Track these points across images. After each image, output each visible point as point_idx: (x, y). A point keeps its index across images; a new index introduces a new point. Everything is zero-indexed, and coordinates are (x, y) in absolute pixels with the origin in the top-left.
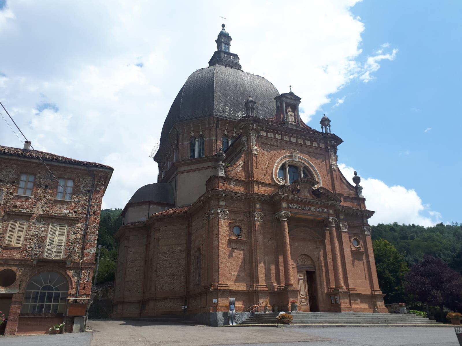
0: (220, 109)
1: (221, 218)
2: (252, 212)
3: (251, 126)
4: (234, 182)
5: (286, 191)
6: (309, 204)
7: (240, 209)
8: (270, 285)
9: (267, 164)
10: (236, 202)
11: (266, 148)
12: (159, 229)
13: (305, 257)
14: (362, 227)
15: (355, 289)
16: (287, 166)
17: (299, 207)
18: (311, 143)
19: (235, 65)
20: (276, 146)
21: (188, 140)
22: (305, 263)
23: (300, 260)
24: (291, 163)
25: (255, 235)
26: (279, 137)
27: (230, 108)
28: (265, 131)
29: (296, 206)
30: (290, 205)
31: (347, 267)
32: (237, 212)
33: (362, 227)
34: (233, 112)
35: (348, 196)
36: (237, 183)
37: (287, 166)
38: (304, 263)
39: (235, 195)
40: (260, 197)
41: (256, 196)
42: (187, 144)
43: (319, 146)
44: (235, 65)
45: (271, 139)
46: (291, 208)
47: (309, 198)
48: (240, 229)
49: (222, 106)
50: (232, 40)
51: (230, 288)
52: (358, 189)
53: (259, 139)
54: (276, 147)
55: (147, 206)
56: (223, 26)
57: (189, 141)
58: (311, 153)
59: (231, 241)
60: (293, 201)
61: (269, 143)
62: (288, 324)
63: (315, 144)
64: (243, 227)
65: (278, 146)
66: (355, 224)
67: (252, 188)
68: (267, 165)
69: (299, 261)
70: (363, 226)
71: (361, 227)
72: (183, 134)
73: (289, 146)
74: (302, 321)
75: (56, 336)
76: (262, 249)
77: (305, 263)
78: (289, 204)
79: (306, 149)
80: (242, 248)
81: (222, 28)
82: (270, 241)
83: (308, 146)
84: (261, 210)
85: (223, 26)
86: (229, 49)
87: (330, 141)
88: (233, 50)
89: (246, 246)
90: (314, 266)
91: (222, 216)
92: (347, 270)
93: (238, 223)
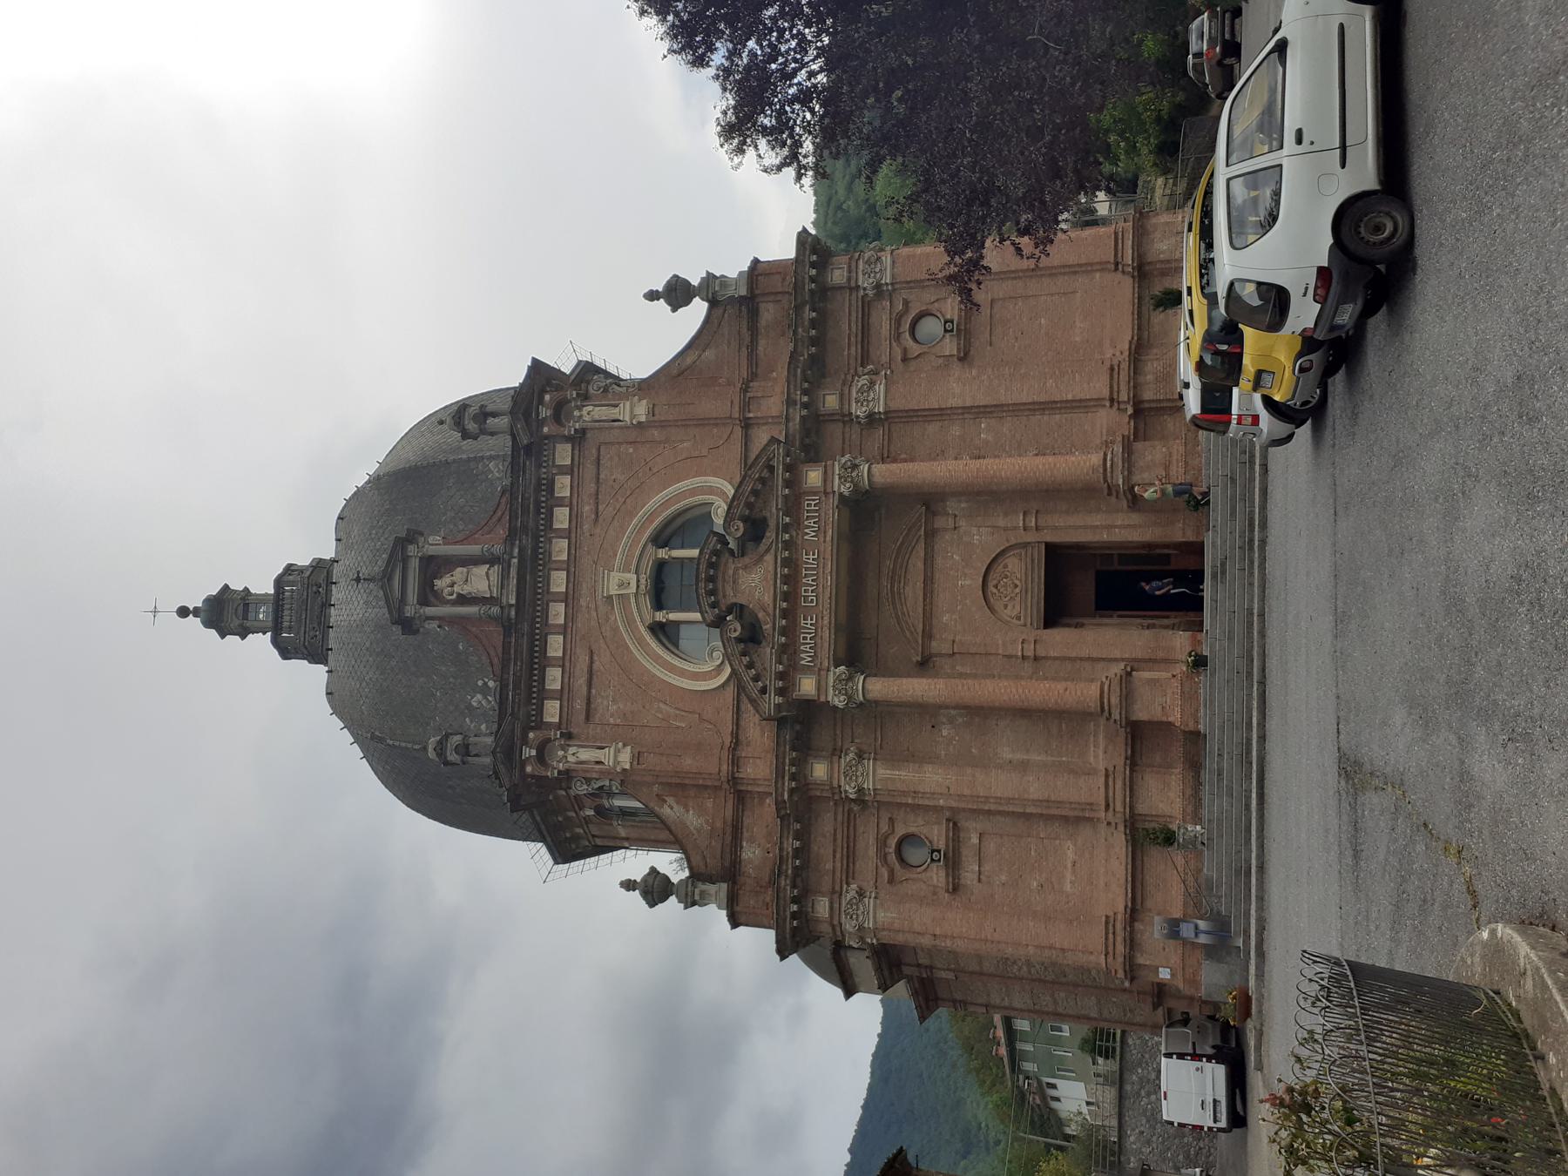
0: (483, 727)
1: (875, 922)
2: (843, 796)
3: (533, 769)
4: (741, 847)
5: (756, 679)
6: (792, 564)
7: (839, 836)
8: (1105, 752)
9: (662, 705)
10: (816, 848)
11: (605, 703)
12: (926, 967)
13: (995, 582)
14: (862, 292)
15: (1112, 369)
16: (660, 616)
17: (809, 622)
18: (560, 502)
19: (315, 588)
20: (592, 662)
21: (612, 825)
22: (1016, 586)
23: (1006, 607)
24: (647, 603)
25: (928, 796)
26: (555, 645)
27: (476, 690)
28: (545, 671)
29: (809, 636)
30: (805, 660)
31: (1025, 397)
32: (848, 848)
33: (862, 292)
34: (486, 680)
35: (744, 350)
36: (746, 834)
37: (660, 616)
38: (1018, 590)
39: (790, 860)
40: (787, 768)
41: (786, 784)
42: (623, 826)
43: (569, 470)
44: (315, 588)
45: (566, 680)
46: (814, 657)
47: (771, 568)
48: (903, 840)
49: (471, 722)
50: (226, 587)
51: (1121, 908)
52: (712, 288)
53: (574, 730)
54: (595, 658)
55: (849, 953)
56: (183, 612)
57: (615, 823)
58: (597, 508)
59: (954, 884)
60: (788, 651)
61: (585, 689)
62: (1248, 999)
63: (563, 486)
64: (900, 831)
65: (592, 653)
66: (854, 330)
67: (758, 785)
68: (668, 708)
69: (1008, 612)
70: (858, 287)
71: (862, 297)
72: (593, 836)
73: (583, 603)
74: (1238, 872)
75: (1269, 588)
76: (974, 776)
77: (1016, 586)
78: (803, 662)
79: (586, 527)
80: (975, 840)
81: (191, 615)
82: (945, 733)
83: (575, 517)
84: (835, 759)
85: (183, 612)
86: (262, 599)
87: (542, 423)
88: (264, 586)
89: (967, 824)
90: (1025, 545)
91: (867, 774)
92: (1036, 398)
93: (887, 850)
